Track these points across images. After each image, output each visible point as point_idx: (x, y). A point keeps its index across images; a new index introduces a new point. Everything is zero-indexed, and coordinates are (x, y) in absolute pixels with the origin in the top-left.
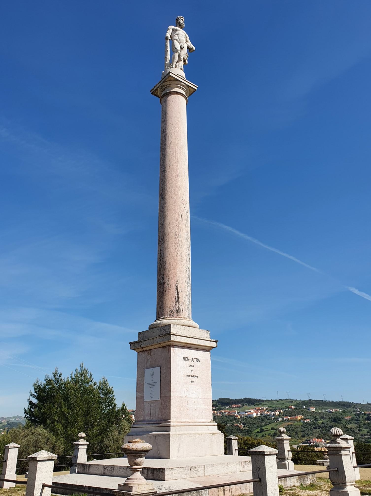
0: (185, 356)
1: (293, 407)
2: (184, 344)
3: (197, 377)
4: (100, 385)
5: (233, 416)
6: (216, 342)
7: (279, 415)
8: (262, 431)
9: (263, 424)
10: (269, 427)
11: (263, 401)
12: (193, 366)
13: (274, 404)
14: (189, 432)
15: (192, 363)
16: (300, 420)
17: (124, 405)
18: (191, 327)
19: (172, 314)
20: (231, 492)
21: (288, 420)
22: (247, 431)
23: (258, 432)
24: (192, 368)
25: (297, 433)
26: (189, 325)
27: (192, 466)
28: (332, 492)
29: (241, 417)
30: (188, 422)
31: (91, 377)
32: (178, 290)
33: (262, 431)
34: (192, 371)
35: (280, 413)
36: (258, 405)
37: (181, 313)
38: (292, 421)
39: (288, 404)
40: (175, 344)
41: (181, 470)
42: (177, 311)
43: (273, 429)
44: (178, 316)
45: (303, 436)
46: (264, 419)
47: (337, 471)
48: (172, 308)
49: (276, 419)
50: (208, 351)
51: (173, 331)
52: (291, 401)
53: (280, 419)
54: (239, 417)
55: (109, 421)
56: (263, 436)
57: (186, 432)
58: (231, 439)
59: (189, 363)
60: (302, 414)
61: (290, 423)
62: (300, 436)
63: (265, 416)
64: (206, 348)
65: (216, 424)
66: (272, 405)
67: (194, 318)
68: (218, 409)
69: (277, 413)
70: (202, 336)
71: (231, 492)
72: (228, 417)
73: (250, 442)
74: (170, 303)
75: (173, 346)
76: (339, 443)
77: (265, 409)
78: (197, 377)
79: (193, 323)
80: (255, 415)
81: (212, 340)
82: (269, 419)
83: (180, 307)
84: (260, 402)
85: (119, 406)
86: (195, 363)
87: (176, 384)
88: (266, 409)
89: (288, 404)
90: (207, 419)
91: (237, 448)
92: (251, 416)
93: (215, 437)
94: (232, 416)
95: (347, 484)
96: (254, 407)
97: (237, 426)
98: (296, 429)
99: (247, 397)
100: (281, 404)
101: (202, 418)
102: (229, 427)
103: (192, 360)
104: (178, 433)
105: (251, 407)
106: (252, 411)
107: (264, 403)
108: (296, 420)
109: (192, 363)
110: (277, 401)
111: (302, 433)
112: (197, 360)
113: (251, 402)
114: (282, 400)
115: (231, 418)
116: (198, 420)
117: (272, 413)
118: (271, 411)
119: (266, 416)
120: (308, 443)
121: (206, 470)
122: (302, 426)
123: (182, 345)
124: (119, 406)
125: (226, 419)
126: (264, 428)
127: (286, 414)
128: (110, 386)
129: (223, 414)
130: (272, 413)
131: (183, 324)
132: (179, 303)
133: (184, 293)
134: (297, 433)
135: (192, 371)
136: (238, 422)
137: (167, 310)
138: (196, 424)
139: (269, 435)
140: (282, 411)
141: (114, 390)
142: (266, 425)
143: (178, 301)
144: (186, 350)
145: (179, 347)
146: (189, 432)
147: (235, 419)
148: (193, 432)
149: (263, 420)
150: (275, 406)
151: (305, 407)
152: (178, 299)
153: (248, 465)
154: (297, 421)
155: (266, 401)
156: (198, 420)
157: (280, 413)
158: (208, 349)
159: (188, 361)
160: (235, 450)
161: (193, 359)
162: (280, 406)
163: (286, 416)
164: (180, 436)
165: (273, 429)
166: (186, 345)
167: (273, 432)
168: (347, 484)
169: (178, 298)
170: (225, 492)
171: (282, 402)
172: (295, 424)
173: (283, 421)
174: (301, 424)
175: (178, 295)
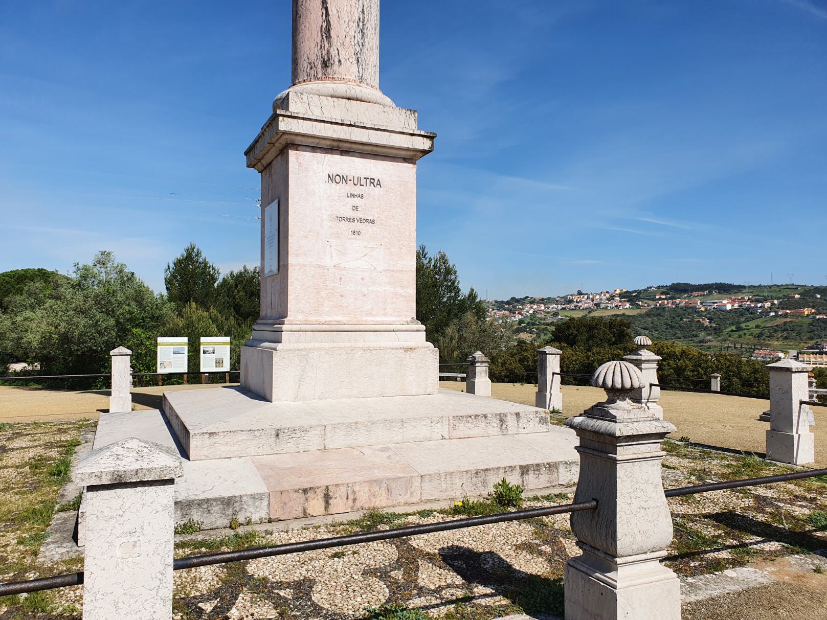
0: (334, 171)
1: (797, 296)
2: (328, 143)
3: (373, 222)
4: (436, 261)
5: (695, 308)
6: (431, 138)
7: (770, 308)
8: (739, 329)
9: (742, 319)
10: (752, 324)
11: (744, 287)
12: (361, 196)
13: (763, 291)
14: (335, 345)
15: (358, 190)
16: (808, 315)
17: (472, 290)
18: (357, 100)
19: (312, 72)
20: (354, 500)
21: (786, 315)
22: (715, 329)
23: (732, 331)
24: (357, 201)
25: (799, 334)
26: (349, 95)
27: (278, 427)
28: (572, 570)
29: (706, 310)
30: (339, 323)
31: (423, 251)
32: (326, 9)
33: (739, 329)
34: (355, 208)
35: (773, 304)
36: (735, 293)
37: (336, 67)
38: (792, 317)
39: (789, 292)
40: (298, 140)
41: (243, 436)
42: (326, 64)
43: (757, 327)
44: (326, 76)
45: (811, 339)
46: (743, 313)
47: (595, 509)
48: (313, 58)
49: (766, 312)
50: (406, 160)
51: (293, 108)
52: (795, 288)
53: (772, 314)
54: (703, 309)
55: (449, 313)
56: (740, 336)
57: (327, 345)
58: (545, 353)
59: (350, 188)
60: (813, 307)
61: (788, 320)
62: (804, 338)
63: (746, 309)
64: (403, 153)
65: (424, 327)
66: (759, 293)
67: (385, 87)
68: (670, 298)
69: (768, 305)
70: (396, 123)
71: (354, 500)
72: (686, 308)
73: (666, 350)
74: (310, 46)
75: (296, 147)
76: (613, 419)
77: (746, 298)
78: (373, 222)
79: (377, 95)
80: (729, 307)
81: (423, 133)
82: (752, 313)
83: (333, 52)
84: (740, 288)
85: (464, 291)
86: (367, 190)
87: (306, 237)
88: (749, 299)
89: (789, 292)
90: (399, 316)
91: (558, 370)
92: (723, 308)
93: (413, 355)
94: (692, 308)
95: (619, 560)
96: (728, 296)
97: (699, 321)
98: (799, 328)
99: (718, 282)
100: (775, 291)
101: (385, 315)
102: (685, 323)
103: (358, 182)
104: (301, 346)
105: (724, 296)
106: (725, 302)
107: (747, 290)
108: (801, 315)
109: (358, 190)
110: (770, 287)
111: (808, 335)
112: (374, 182)
113: (724, 289)
114: (778, 286)
115: (690, 310)
116: (370, 319)
117: (759, 305)
118: (758, 301)
119: (748, 309)
120: (817, 348)
121: (328, 435)
122: (811, 324)
123: (324, 144)
124: (464, 291)
125: (681, 312)
126: (743, 325)
127: (782, 306)
128: (451, 263)
129: (677, 305)
130: (759, 305)
131: (332, 92)
132: (330, 43)
133: (344, 15)
134: (799, 334)
135: (355, 208)
136: (701, 316)
137: (304, 64)
138: (362, 327)
139: (751, 335)
140: (776, 302)
141: (457, 268)
142: (747, 320)
143: (329, 37)
144: (337, 158)
145: (314, 149)
146: (335, 345)
147: (696, 312)
148: (347, 344)
149: (742, 315)
150: (766, 294)
151: (819, 296)
152: (327, 32)
153: (469, 425)
154: (803, 317)
155: (749, 287)
156: (370, 319)
157: (773, 304)
158: (410, 157)
159: (342, 185)
160: (554, 374)
161: (359, 179)
162: (774, 295)
163: (783, 309)
164: (304, 353)
165: (757, 327)
166: (335, 144)
167: (757, 331)
168: (619, 560)
169: (328, 30)
170: (331, 501)
171: (778, 289)
172: (797, 321)
173: (777, 316)
174: (809, 321)
175: (328, 22)
